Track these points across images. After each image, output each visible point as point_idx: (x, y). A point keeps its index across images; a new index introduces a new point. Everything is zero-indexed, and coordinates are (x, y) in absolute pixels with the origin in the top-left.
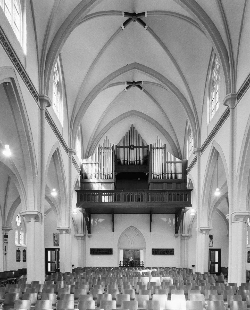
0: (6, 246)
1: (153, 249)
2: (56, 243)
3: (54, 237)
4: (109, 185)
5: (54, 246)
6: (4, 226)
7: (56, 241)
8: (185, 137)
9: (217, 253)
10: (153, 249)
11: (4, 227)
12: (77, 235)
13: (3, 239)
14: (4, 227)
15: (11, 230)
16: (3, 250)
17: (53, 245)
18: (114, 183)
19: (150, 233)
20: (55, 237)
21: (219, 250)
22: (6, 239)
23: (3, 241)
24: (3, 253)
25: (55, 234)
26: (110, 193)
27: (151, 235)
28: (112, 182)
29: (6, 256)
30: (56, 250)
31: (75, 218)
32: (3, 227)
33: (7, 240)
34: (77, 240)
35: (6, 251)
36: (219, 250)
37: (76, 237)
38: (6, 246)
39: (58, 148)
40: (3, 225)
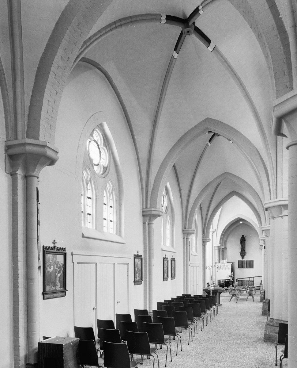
6: (147, 208)
11: (16, 142)
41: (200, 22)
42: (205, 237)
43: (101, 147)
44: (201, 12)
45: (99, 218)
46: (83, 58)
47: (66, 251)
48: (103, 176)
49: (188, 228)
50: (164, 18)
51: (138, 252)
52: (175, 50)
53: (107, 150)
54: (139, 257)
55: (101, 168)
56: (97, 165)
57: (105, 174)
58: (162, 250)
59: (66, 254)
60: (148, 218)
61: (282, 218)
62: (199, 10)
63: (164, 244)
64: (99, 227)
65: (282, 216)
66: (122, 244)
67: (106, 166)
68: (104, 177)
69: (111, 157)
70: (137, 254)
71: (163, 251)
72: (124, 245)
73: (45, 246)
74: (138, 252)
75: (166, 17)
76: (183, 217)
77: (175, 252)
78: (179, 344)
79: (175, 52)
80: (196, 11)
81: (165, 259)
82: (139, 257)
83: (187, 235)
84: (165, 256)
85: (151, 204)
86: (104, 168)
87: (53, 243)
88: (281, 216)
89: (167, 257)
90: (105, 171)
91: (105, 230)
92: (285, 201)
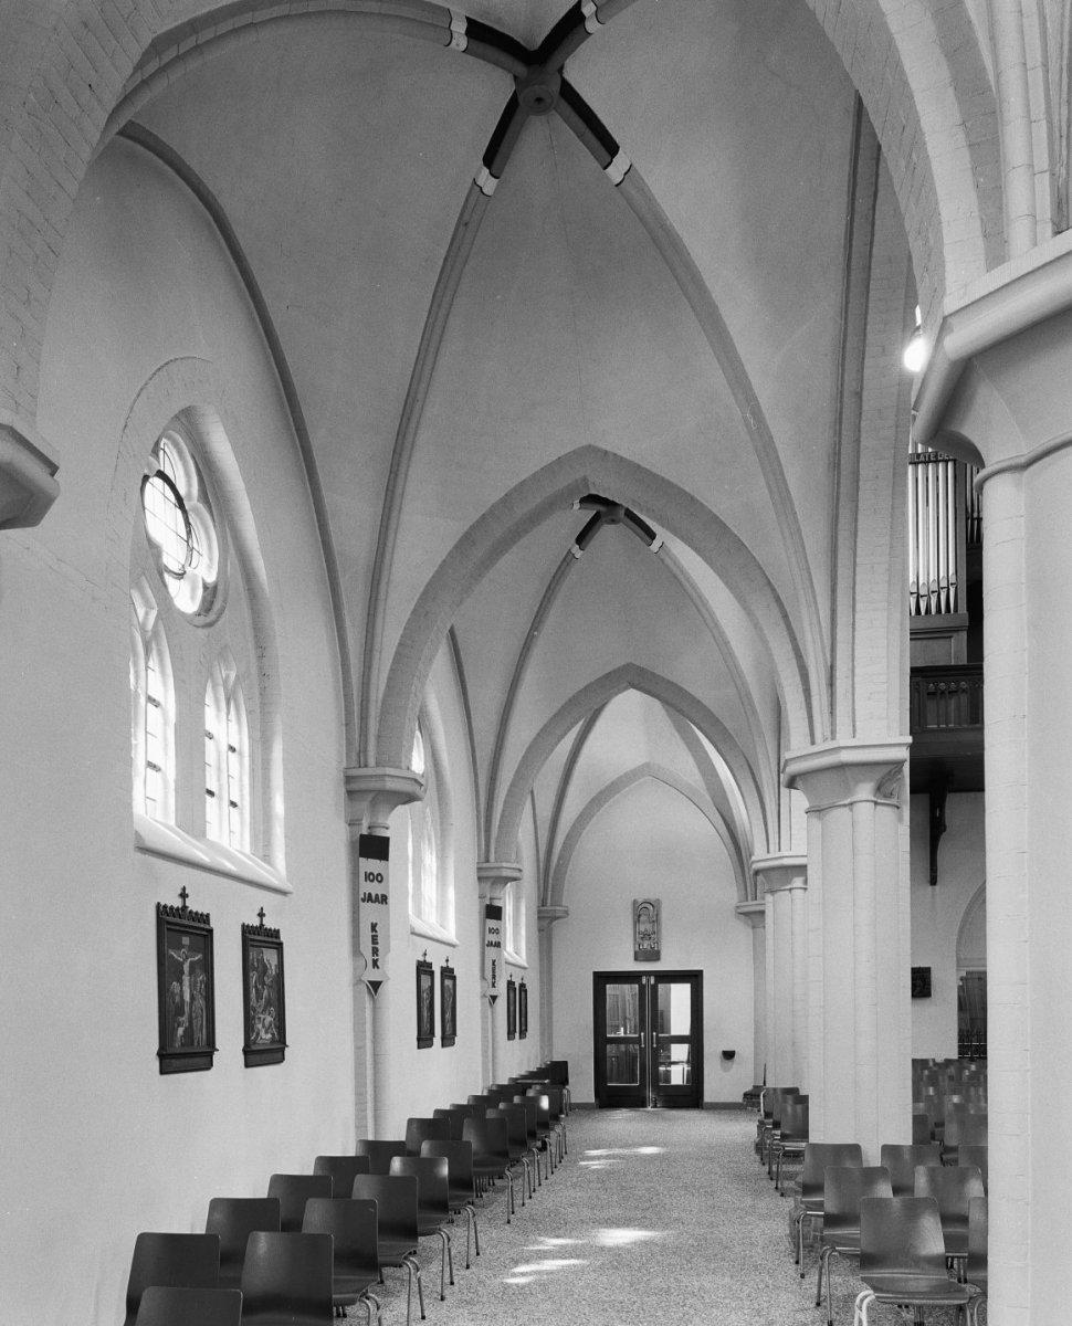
0: (494, 962)
1: (928, 970)
2: (646, 945)
3: (637, 920)
4: (941, 642)
5: (636, 959)
6: (488, 861)
7: (646, 936)
8: (401, 434)
9: (680, 995)
10: (928, 970)
11: (487, 865)
12: (750, 903)
13: (483, 925)
14: (487, 865)
15: (515, 879)
16: (483, 978)
17: (633, 958)
18: (964, 635)
19: (930, 888)
20: (639, 916)
21: (694, 978)
22: (492, 923)
23: (484, 940)
24: (484, 996)
25: (640, 901)
26: (957, 682)
27: (933, 896)
28: (957, 630)
29: (375, 1009)
30: (644, 980)
31: (378, 829)
32: (480, 866)
33: (496, 931)
34: (750, 931)
35: (493, 986)
36: (694, 978)
37: (746, 914)
38: (494, 962)
39: (53, 474)
40: (483, 859)
41: (585, 71)
42: (372, 761)
43: (192, 503)
44: (591, 25)
45: (193, 792)
46: (131, 123)
47: (282, 939)
48: (202, 620)
49: (378, 764)
50: (459, 27)
51: (447, 961)
52: (489, 159)
53: (212, 515)
54: (266, 939)
55: (193, 590)
56: (180, 576)
57: (212, 616)
58: (412, 933)
59: (281, 944)
60: (364, 805)
61: (851, 810)
62: (583, 18)
63: (419, 914)
64: (192, 821)
65: (851, 804)
66: (279, 897)
67: (211, 578)
68: (210, 625)
69: (232, 551)
70: (255, 922)
71: (414, 937)
72: (287, 899)
73: (163, 904)
74: (261, 915)
75: (466, 25)
76: (478, 805)
77: (284, 893)
78: (412, 1300)
79: (486, 171)
80: (571, 26)
81: (423, 968)
82: (266, 939)
83: (493, 884)
84: (447, 961)
85: (379, 753)
86: (205, 587)
87: (187, 896)
88: (788, 887)
89: (428, 960)
90: (207, 606)
91: (213, 833)
92: (867, 751)
